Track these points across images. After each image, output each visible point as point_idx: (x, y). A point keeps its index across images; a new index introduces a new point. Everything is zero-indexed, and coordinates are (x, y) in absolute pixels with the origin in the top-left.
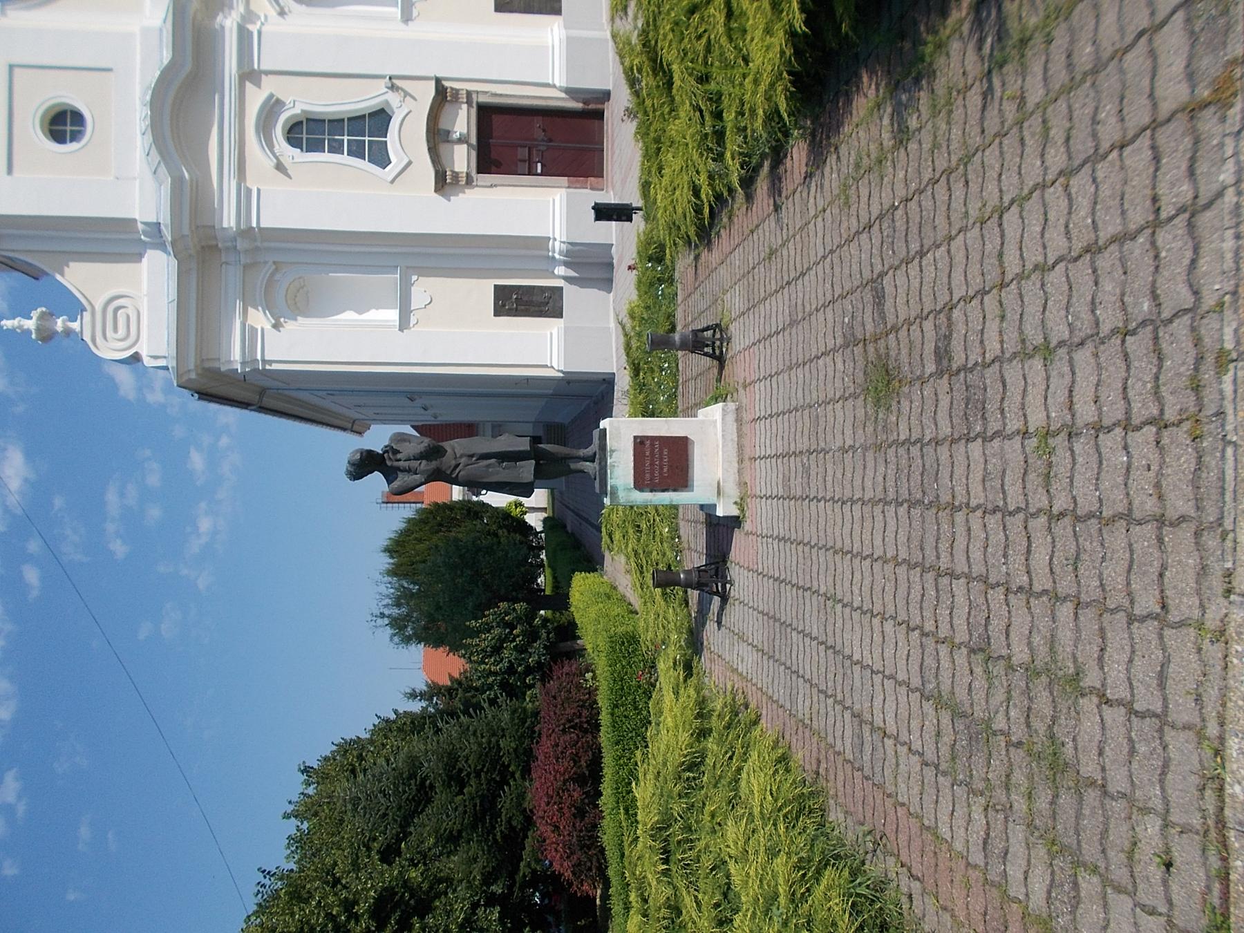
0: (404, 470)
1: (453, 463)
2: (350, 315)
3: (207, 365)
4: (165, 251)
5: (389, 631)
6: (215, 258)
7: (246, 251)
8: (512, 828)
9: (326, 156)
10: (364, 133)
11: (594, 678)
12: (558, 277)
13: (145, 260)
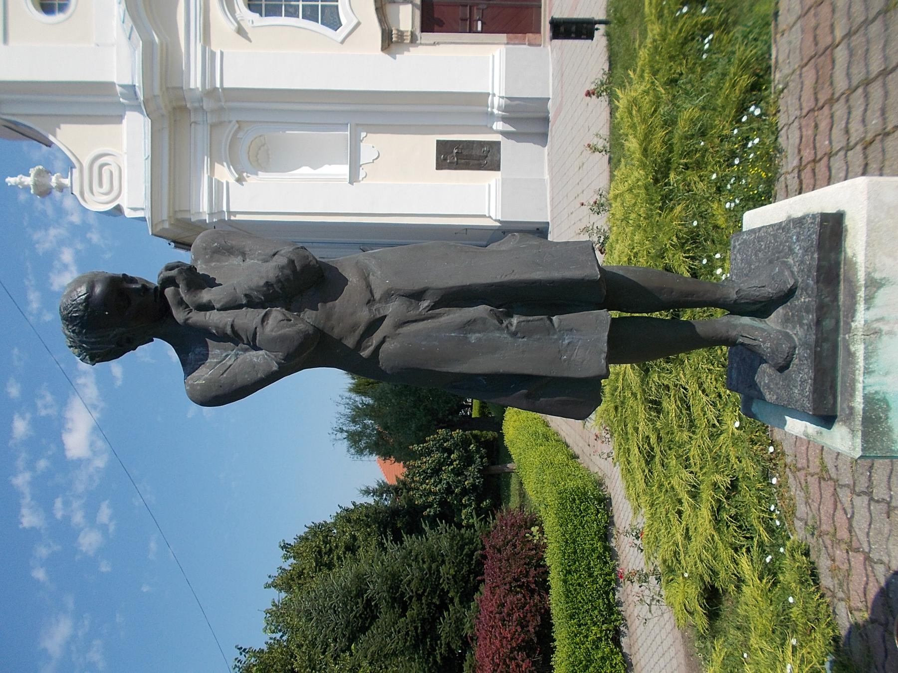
0: (222, 337)
1: (364, 316)
2: (305, 170)
3: (179, 216)
4: (142, 113)
5: (346, 443)
7: (213, 111)
8: (450, 650)
9: (283, 20)
11: (541, 531)
12: (495, 132)
13: (125, 121)
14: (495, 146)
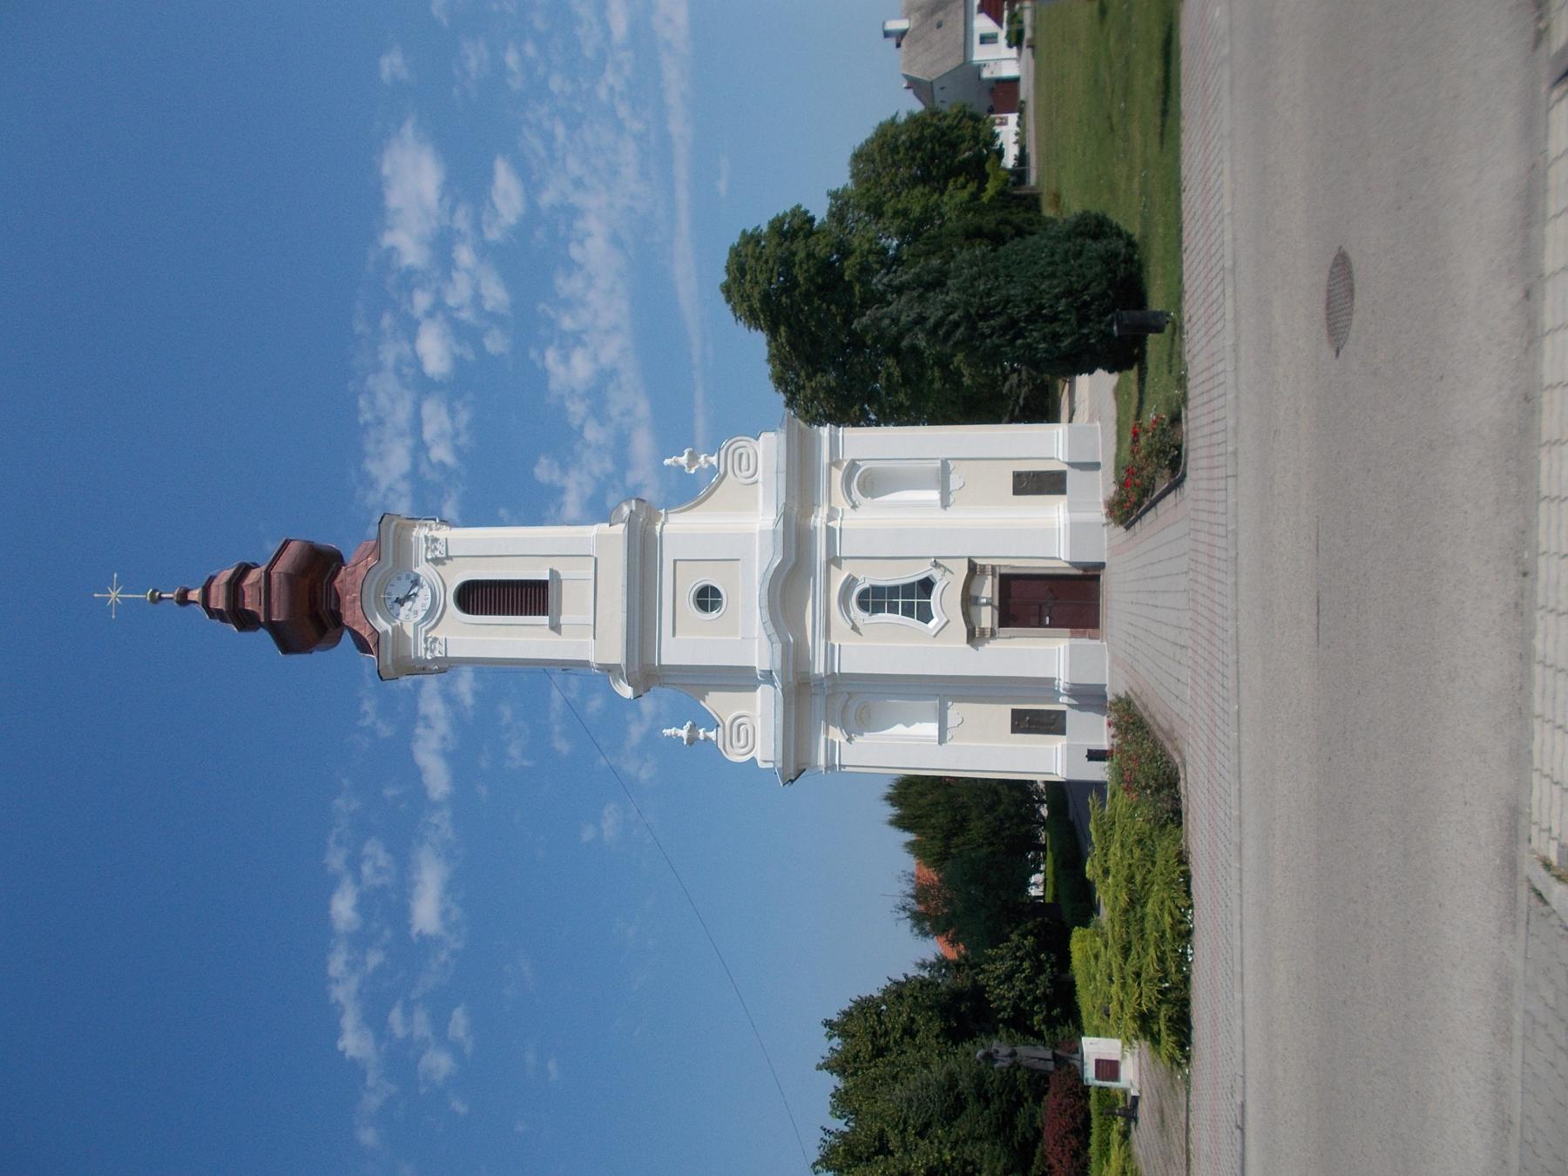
2: (899, 729)
6: (812, 696)
10: (913, 598)
14: (1061, 715)
